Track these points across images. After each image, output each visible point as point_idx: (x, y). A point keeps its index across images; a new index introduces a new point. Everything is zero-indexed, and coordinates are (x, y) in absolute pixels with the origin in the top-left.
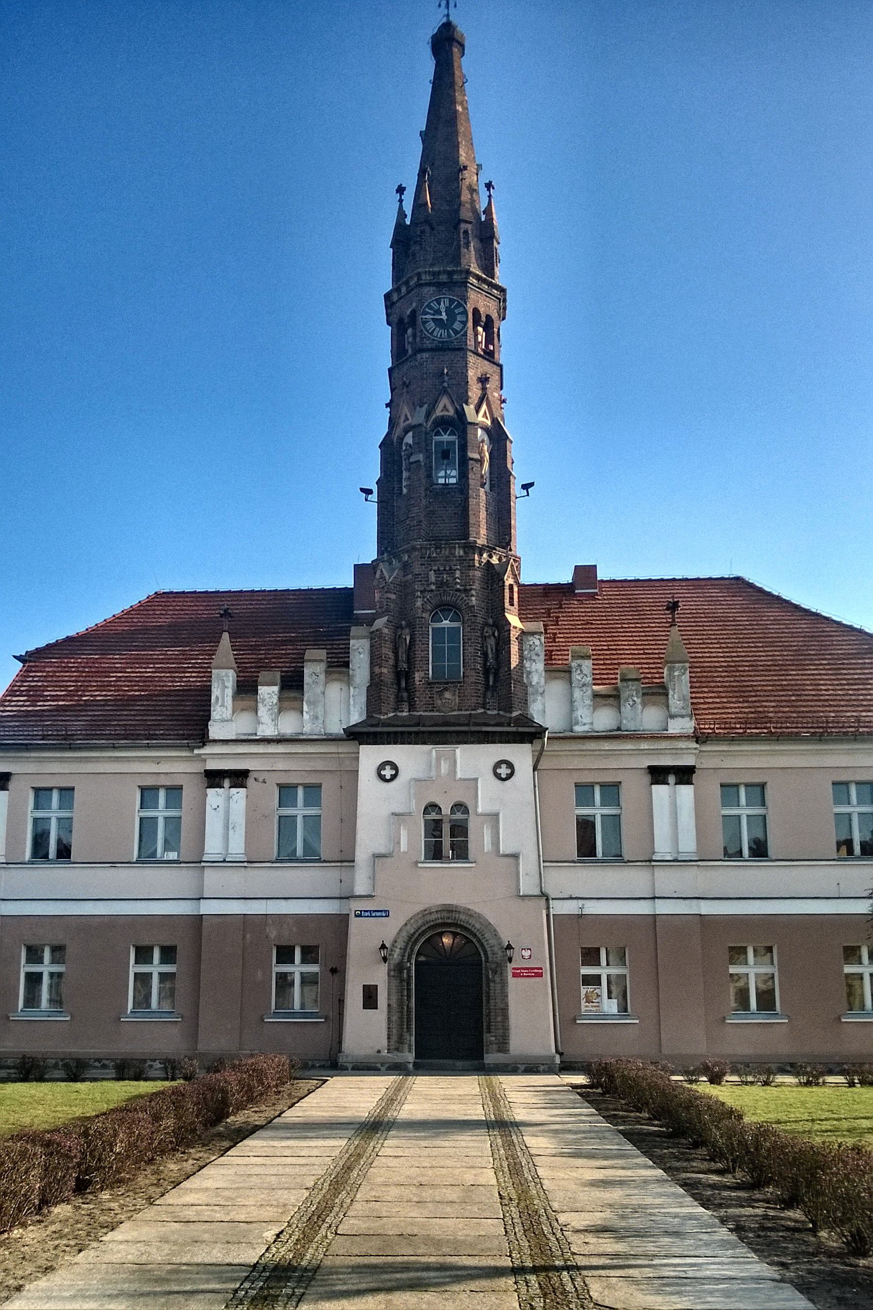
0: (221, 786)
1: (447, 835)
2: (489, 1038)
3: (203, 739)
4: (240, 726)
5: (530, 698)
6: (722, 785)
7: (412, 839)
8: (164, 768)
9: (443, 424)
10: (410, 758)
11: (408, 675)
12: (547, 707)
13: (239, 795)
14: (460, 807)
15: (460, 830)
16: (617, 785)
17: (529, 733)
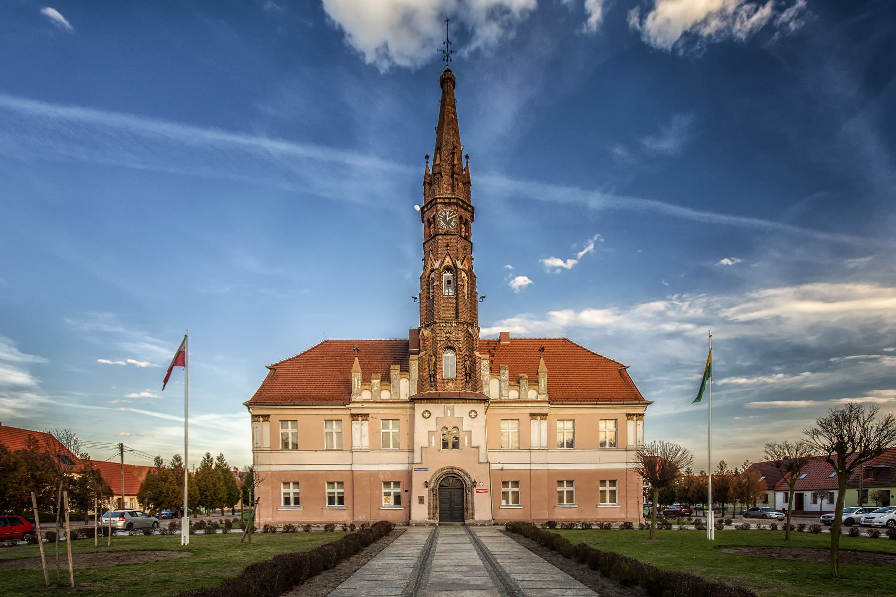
1: (451, 444)
3: (350, 401)
4: (366, 395)
7: (436, 442)
8: (334, 412)
10: (437, 410)
17: (486, 400)
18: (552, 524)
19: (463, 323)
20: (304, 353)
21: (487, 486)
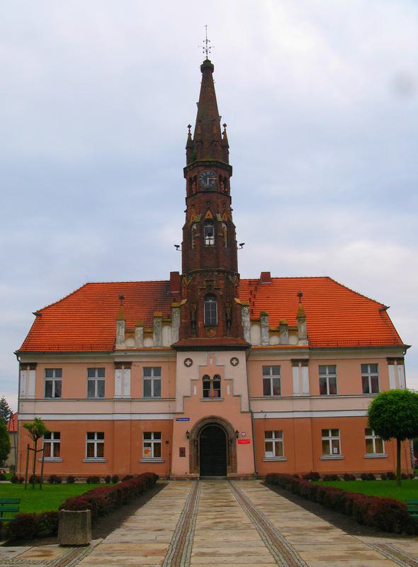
0: (298, 366)
1: (211, 386)
2: (228, 467)
4: (130, 343)
5: (244, 332)
6: (319, 366)
7: (198, 390)
9: (209, 221)
10: (200, 359)
11: (195, 323)
12: (254, 335)
13: (128, 371)
14: (217, 376)
15: (217, 385)
16: (279, 367)
17: (245, 347)
18: (314, 476)
19: (223, 272)
20: (68, 297)
21: (249, 436)
